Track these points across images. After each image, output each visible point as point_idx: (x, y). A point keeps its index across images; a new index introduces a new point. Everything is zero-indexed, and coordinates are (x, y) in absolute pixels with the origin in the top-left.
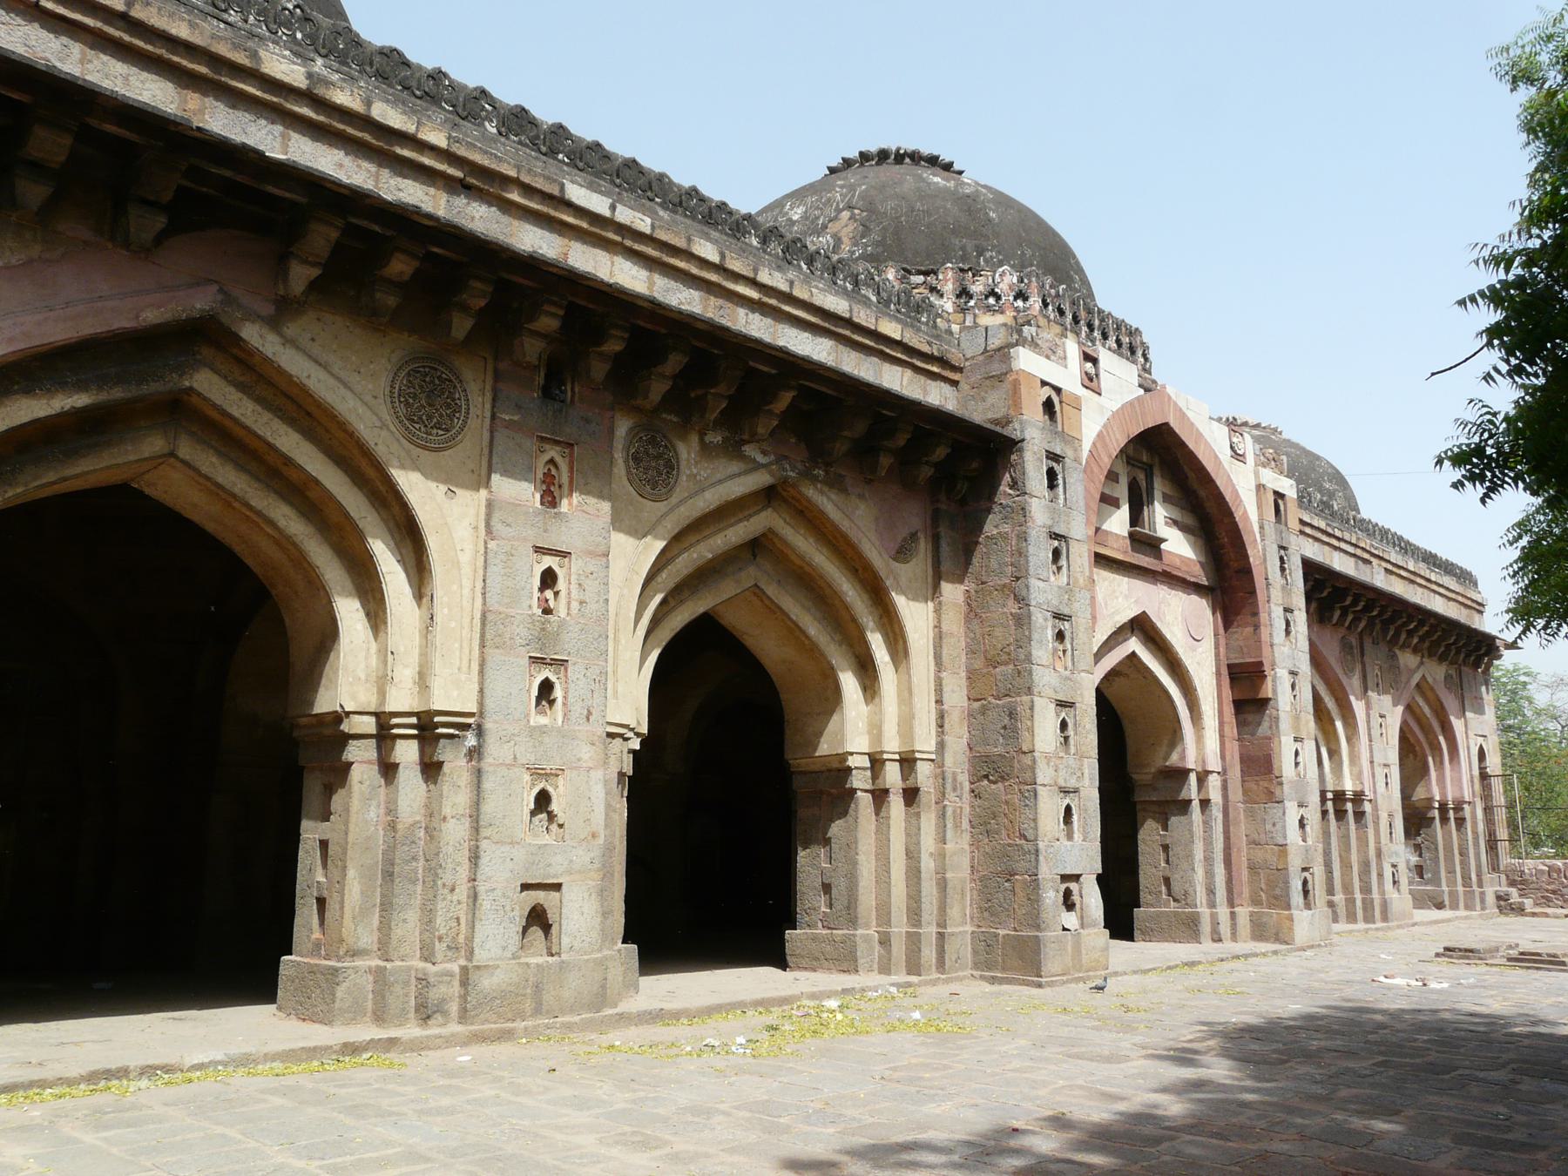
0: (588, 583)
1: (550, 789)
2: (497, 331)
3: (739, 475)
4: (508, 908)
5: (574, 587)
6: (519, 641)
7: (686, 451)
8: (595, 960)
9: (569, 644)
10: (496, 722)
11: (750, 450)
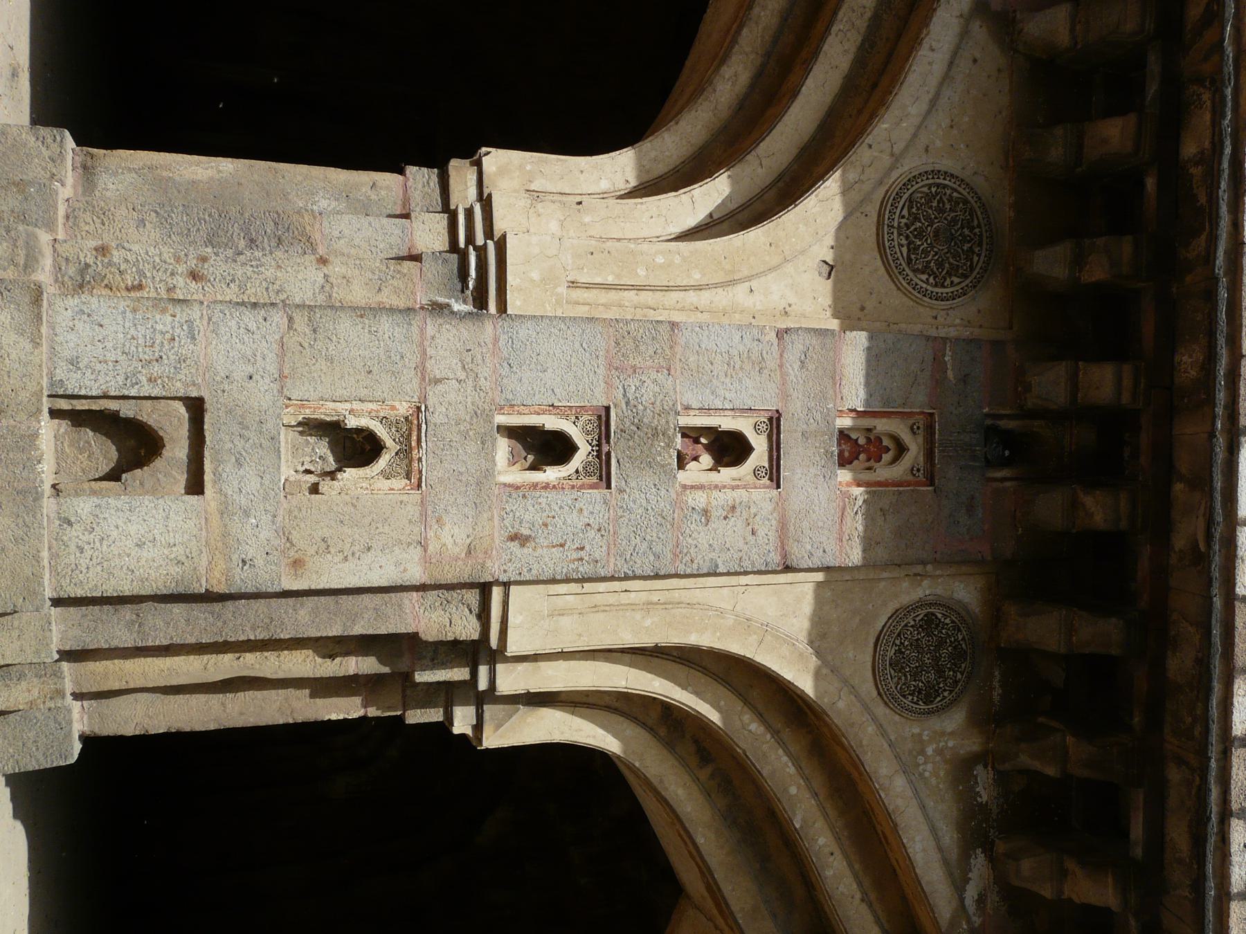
0: (736, 523)
1: (383, 462)
2: (1056, 323)
3: (940, 849)
4: (156, 369)
5: (729, 496)
6: (633, 383)
7: (951, 729)
8: (38, 577)
9: (638, 489)
10: (496, 340)
11: (979, 862)
